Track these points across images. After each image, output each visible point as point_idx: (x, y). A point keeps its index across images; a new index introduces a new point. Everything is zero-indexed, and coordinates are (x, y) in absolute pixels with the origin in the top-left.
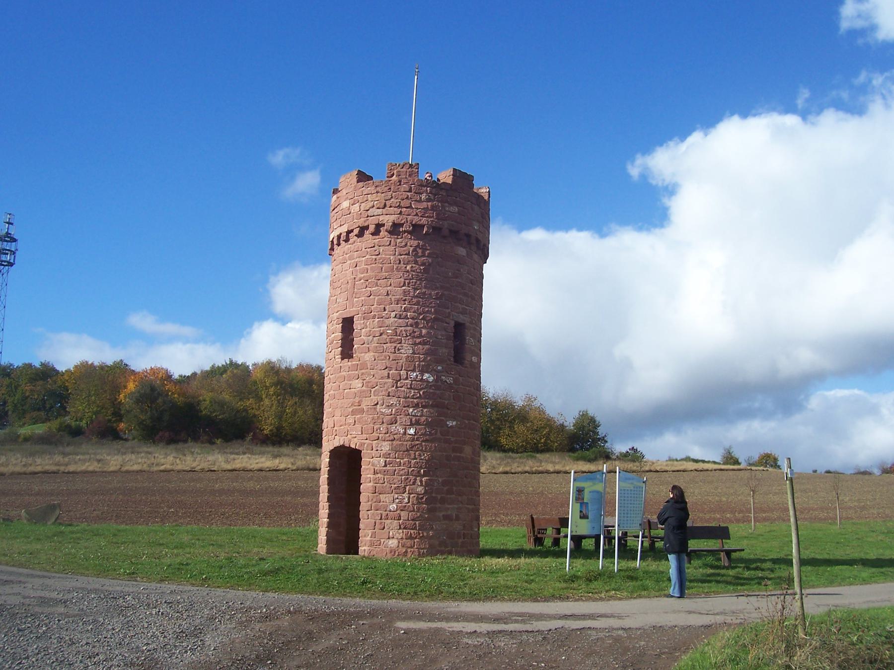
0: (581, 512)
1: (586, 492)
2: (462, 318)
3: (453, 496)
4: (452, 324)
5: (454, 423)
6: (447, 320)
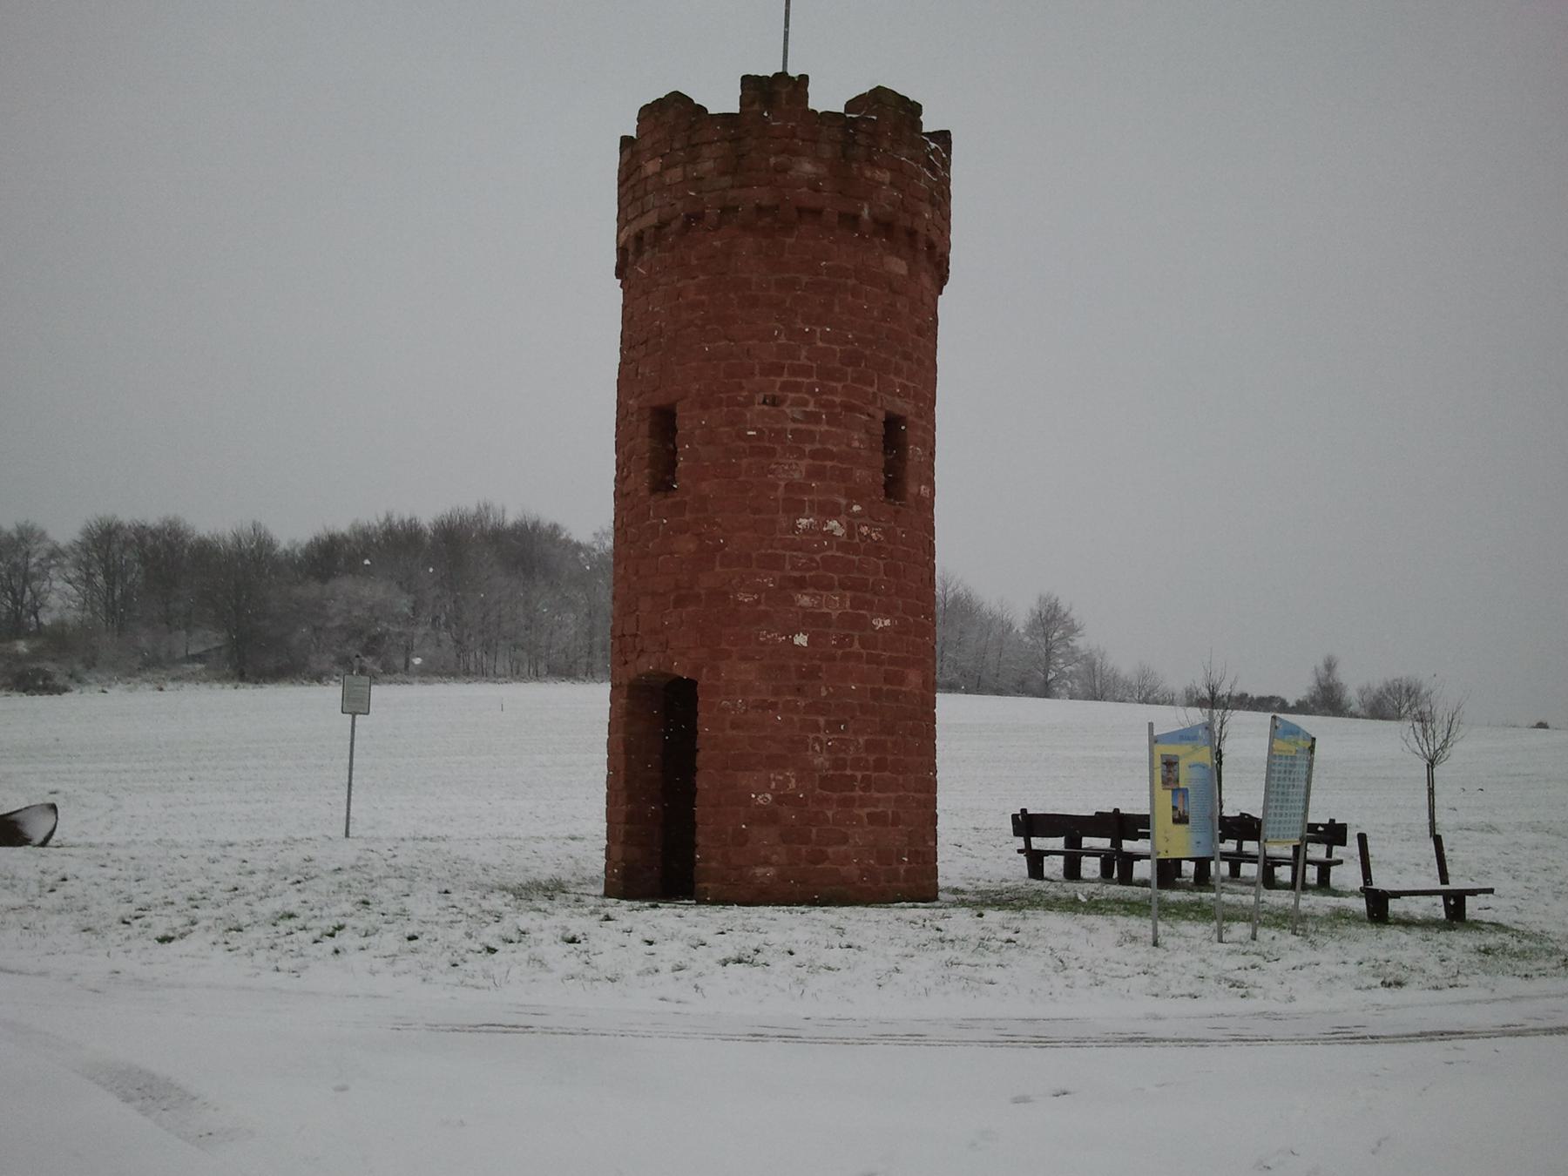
0: (1175, 808)
1: (1182, 764)
2: (903, 406)
3: (887, 773)
4: (881, 416)
5: (887, 622)
6: (871, 410)
